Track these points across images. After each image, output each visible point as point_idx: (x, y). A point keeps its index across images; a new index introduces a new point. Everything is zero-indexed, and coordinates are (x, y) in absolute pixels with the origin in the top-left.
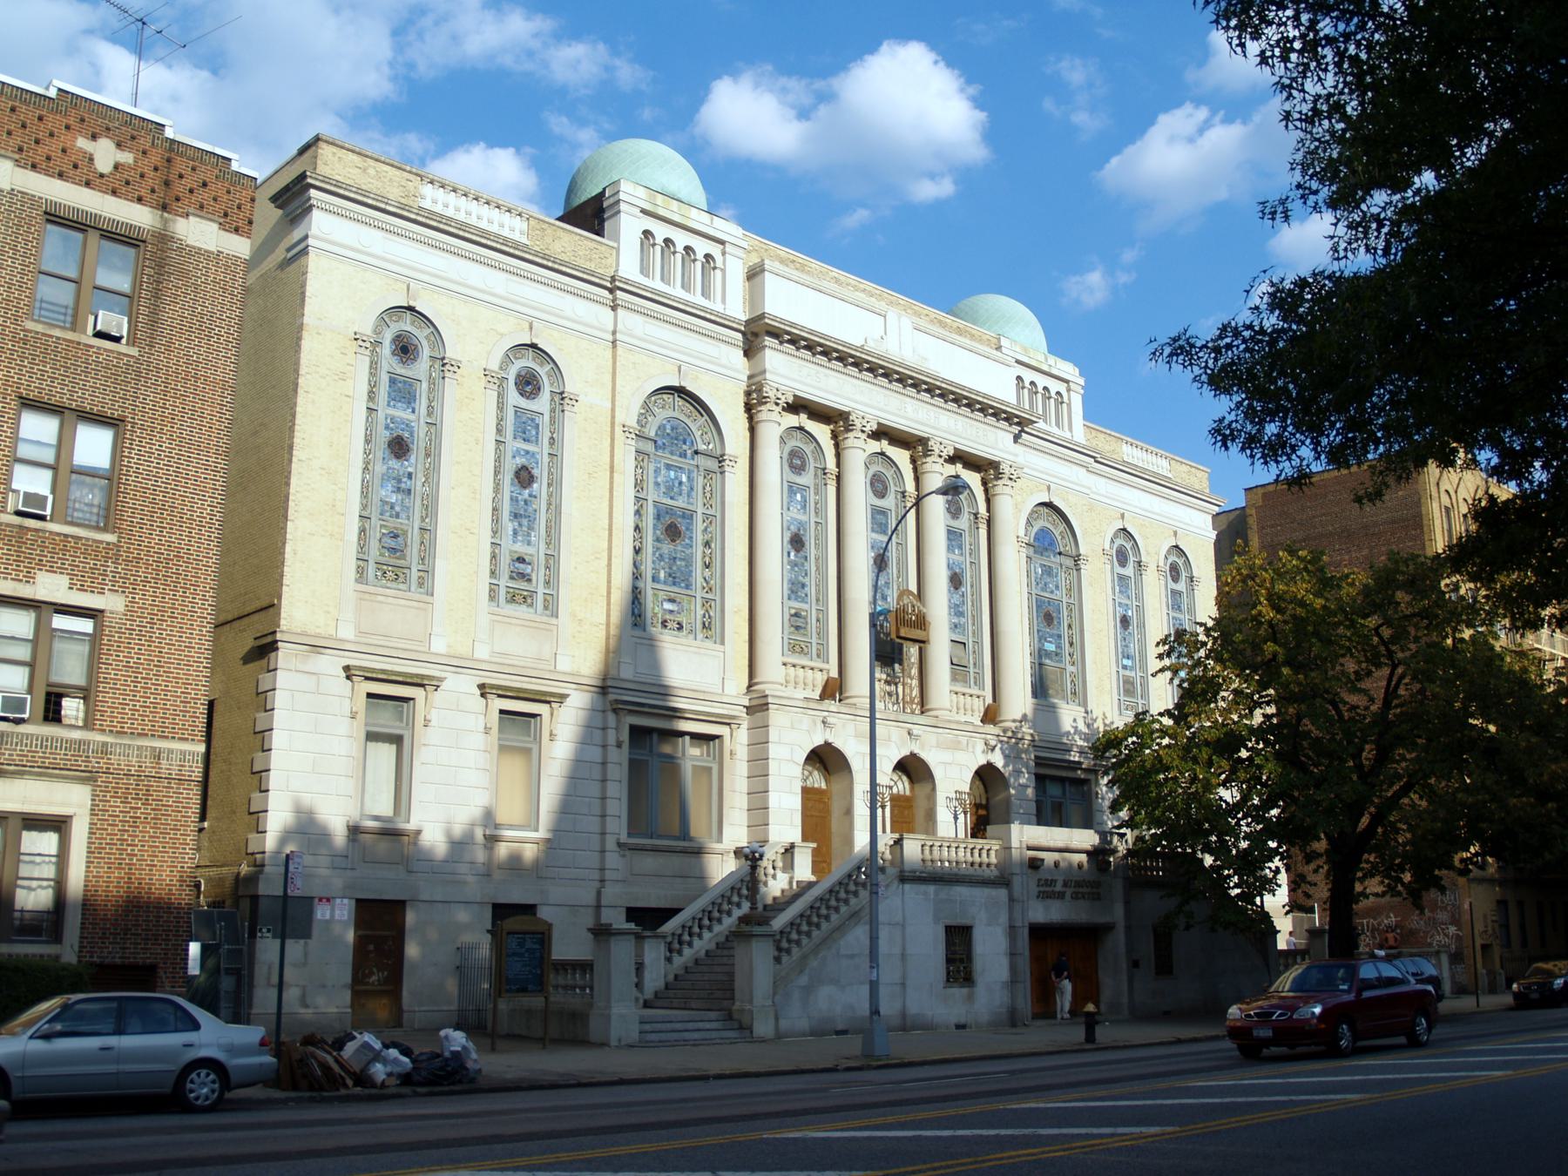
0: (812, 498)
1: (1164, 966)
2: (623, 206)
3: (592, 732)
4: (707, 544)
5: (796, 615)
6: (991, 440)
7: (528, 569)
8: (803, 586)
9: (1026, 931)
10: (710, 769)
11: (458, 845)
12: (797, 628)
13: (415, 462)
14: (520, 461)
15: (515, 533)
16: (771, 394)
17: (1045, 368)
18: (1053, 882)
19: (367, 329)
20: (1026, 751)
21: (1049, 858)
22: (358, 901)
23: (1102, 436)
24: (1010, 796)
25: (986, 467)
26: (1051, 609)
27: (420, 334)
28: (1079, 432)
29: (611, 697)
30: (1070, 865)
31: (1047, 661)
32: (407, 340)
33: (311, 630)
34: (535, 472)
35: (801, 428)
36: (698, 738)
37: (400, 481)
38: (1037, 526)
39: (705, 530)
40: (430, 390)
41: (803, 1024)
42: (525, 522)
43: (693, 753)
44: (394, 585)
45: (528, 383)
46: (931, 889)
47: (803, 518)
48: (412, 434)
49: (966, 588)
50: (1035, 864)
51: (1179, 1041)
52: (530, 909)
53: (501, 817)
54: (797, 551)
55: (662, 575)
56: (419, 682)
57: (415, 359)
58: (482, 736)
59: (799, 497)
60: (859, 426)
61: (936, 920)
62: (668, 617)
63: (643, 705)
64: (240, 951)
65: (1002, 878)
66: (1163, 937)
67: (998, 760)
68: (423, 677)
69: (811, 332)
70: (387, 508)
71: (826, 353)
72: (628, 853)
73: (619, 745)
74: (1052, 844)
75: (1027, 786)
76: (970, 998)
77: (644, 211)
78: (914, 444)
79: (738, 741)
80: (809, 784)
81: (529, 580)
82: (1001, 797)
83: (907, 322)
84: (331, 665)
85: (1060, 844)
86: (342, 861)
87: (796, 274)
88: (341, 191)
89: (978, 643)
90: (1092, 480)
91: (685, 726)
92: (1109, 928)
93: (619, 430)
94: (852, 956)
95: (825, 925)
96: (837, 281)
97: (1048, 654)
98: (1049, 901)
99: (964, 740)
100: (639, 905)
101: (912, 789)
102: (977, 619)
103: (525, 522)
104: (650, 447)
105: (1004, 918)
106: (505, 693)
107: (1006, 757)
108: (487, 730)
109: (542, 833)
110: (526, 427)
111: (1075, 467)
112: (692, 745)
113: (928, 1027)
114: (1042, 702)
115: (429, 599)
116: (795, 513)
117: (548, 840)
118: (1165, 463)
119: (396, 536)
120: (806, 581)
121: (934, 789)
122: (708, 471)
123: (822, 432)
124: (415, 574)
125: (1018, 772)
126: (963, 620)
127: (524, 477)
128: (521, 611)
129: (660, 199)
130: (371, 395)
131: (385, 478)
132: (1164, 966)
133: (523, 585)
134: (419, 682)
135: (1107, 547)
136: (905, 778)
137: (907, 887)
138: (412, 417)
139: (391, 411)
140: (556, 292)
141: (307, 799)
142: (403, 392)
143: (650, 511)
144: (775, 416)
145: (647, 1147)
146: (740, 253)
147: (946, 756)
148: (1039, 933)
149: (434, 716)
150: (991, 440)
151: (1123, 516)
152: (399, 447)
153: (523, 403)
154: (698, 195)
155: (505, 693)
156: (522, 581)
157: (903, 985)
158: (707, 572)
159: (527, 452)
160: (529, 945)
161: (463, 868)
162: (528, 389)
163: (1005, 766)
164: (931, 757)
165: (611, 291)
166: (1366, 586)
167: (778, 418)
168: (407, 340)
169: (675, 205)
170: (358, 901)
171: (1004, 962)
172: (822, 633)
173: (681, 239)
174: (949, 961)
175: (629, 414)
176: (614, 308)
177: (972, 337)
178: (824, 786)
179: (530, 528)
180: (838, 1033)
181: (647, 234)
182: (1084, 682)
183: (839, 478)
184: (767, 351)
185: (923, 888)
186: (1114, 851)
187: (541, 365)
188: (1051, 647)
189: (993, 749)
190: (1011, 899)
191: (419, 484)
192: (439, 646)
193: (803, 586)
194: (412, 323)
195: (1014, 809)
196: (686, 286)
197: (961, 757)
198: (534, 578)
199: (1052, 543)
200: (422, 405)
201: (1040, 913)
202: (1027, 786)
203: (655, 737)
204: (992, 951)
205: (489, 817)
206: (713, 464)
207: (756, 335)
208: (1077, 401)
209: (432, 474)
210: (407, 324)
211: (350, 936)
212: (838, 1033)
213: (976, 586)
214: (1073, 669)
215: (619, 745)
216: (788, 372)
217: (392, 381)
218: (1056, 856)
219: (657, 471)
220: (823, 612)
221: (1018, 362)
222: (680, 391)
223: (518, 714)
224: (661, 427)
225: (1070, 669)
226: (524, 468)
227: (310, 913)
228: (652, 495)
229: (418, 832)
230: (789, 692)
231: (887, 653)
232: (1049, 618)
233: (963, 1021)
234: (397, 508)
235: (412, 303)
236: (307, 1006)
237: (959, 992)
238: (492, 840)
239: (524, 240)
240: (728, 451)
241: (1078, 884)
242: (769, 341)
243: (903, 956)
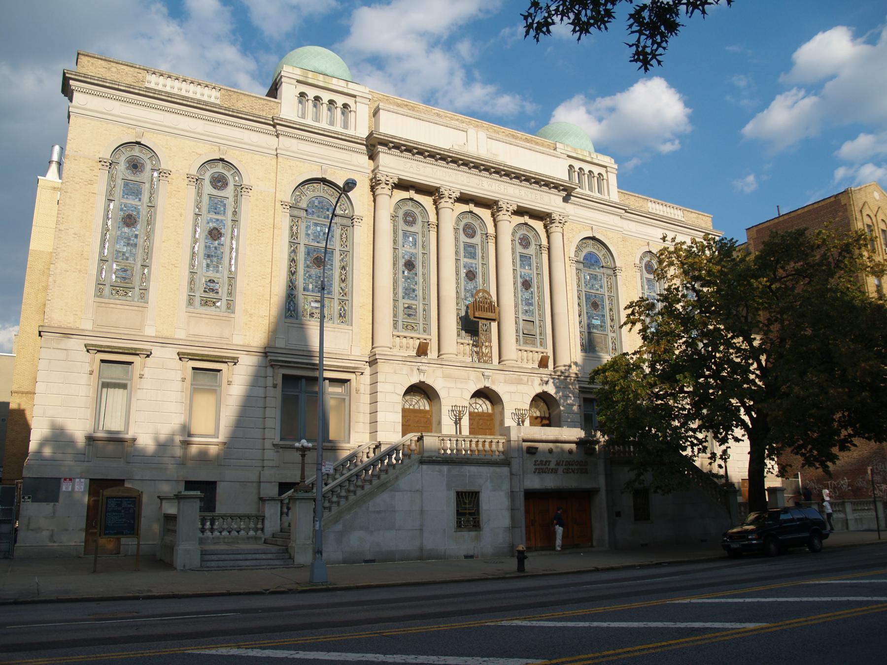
0: (420, 238)
1: (642, 513)
2: (283, 79)
3: (257, 379)
4: (611, 310)
5: (408, 307)
6: (550, 202)
7: (217, 286)
8: (414, 290)
9: (522, 494)
10: (344, 399)
11: (163, 446)
12: (409, 315)
13: (139, 229)
14: (211, 225)
15: (208, 266)
16: (383, 179)
17: (589, 159)
18: (548, 462)
19: (194, 171)
20: (572, 384)
21: (540, 446)
22: (91, 480)
23: (633, 198)
24: (561, 411)
25: (543, 217)
26: (597, 299)
27: (144, 156)
28: (613, 194)
29: (269, 358)
30: (563, 451)
31: (595, 331)
32: (134, 161)
33: (64, 324)
34: (223, 231)
35: (526, 224)
36: (333, 381)
37: (129, 239)
38: (585, 252)
39: (342, 259)
40: (482, 250)
41: (339, 556)
42: (215, 259)
43: (332, 390)
44: (124, 298)
45: (219, 181)
46: (445, 468)
47: (414, 251)
48: (138, 213)
49: (534, 289)
50: (532, 451)
51: (633, 567)
52: (120, 482)
53: (194, 431)
54: (410, 270)
55: (311, 286)
56: (134, 353)
57: (142, 171)
58: (86, 376)
59: (411, 239)
60: (505, 208)
61: (449, 488)
62: (314, 311)
63: (290, 362)
64: (11, 510)
65: (505, 460)
66: (641, 497)
67: (551, 389)
68: (136, 349)
69: (407, 140)
70: (120, 255)
71: (518, 177)
72: (281, 450)
73: (275, 386)
74: (544, 438)
75: (573, 405)
76: (478, 538)
77: (298, 81)
78: (490, 204)
79: (361, 383)
80: (407, 406)
81: (217, 293)
82: (556, 412)
83: (482, 135)
84: (171, 353)
85: (551, 438)
86: (81, 456)
87: (411, 113)
88: (89, 80)
89: (542, 320)
90: (626, 224)
91: (327, 374)
92: (596, 491)
93: (567, 259)
94: (379, 512)
95: (359, 492)
96: (438, 115)
97: (595, 327)
98: (544, 475)
99: (525, 378)
100: (288, 481)
101: (493, 409)
102: (541, 307)
103: (215, 259)
104: (581, 266)
105: (506, 486)
106: (193, 357)
107: (557, 387)
108: (183, 380)
109: (221, 438)
110: (216, 206)
111: (611, 216)
112: (330, 386)
113: (442, 557)
114: (591, 355)
115: (145, 305)
116: (408, 248)
117: (225, 443)
118: (680, 213)
119: (125, 271)
120: (416, 287)
121: (503, 408)
122: (344, 226)
123: (538, 225)
124: (421, 326)
125: (566, 397)
126: (531, 308)
127: (215, 234)
128: (211, 310)
129: (310, 75)
130: (457, 253)
131: (118, 239)
132: (642, 513)
133: (212, 295)
134: (134, 353)
135: (637, 262)
136: (487, 402)
137: (424, 467)
138: (139, 203)
139: (124, 201)
140: (237, 129)
141: (60, 421)
142: (216, 206)
143: (302, 250)
144: (507, 217)
145: (773, 586)
146: (367, 101)
147: (513, 388)
148: (531, 495)
149: (146, 372)
150: (550, 202)
151: (648, 244)
152: (129, 220)
153: (215, 192)
154: (347, 75)
155: (193, 357)
156: (211, 292)
157: (421, 530)
158: (343, 285)
159: (218, 220)
160: (124, 504)
161: (166, 460)
162: (219, 184)
163: (556, 393)
164: (499, 388)
165: (274, 126)
166: (832, 278)
167: (509, 219)
168: (134, 161)
169: (321, 77)
170: (91, 480)
171: (507, 515)
172: (427, 317)
173: (587, 168)
174: (459, 514)
175: (286, 194)
176: (277, 136)
177: (537, 144)
178: (427, 408)
179: (219, 263)
180: (366, 561)
181: (571, 166)
182: (621, 342)
183: (549, 249)
184: (381, 154)
185: (437, 467)
186: (598, 442)
187: (229, 171)
188: (596, 322)
189: (547, 383)
190: (511, 474)
191: (142, 240)
192: (150, 331)
193: (414, 290)
194: (223, 168)
195: (563, 419)
196: (591, 189)
197: (521, 388)
198: (220, 290)
199: (597, 261)
200: (145, 197)
201: (535, 482)
202: (573, 405)
203: (304, 381)
204: (497, 509)
205: (186, 431)
206: (610, 272)
207: (374, 145)
208: (613, 179)
209: (149, 236)
210: (220, 168)
211: (86, 499)
212: (366, 561)
213: (540, 288)
214: (613, 335)
215: (275, 386)
216: (393, 165)
217: (126, 185)
218: (551, 445)
219: (308, 227)
220: (426, 305)
221: (569, 156)
222: (593, 238)
223: (206, 368)
224: (311, 202)
225: (611, 335)
226: (215, 228)
227: (59, 487)
228: (303, 240)
229: (134, 440)
230: (395, 351)
231: (470, 326)
232: (595, 305)
233: (471, 553)
234: (127, 255)
235: (138, 140)
236: (54, 542)
237: (467, 535)
238: (186, 444)
239: (218, 102)
240: (617, 265)
241: (568, 463)
242: (380, 148)
243: (422, 512)
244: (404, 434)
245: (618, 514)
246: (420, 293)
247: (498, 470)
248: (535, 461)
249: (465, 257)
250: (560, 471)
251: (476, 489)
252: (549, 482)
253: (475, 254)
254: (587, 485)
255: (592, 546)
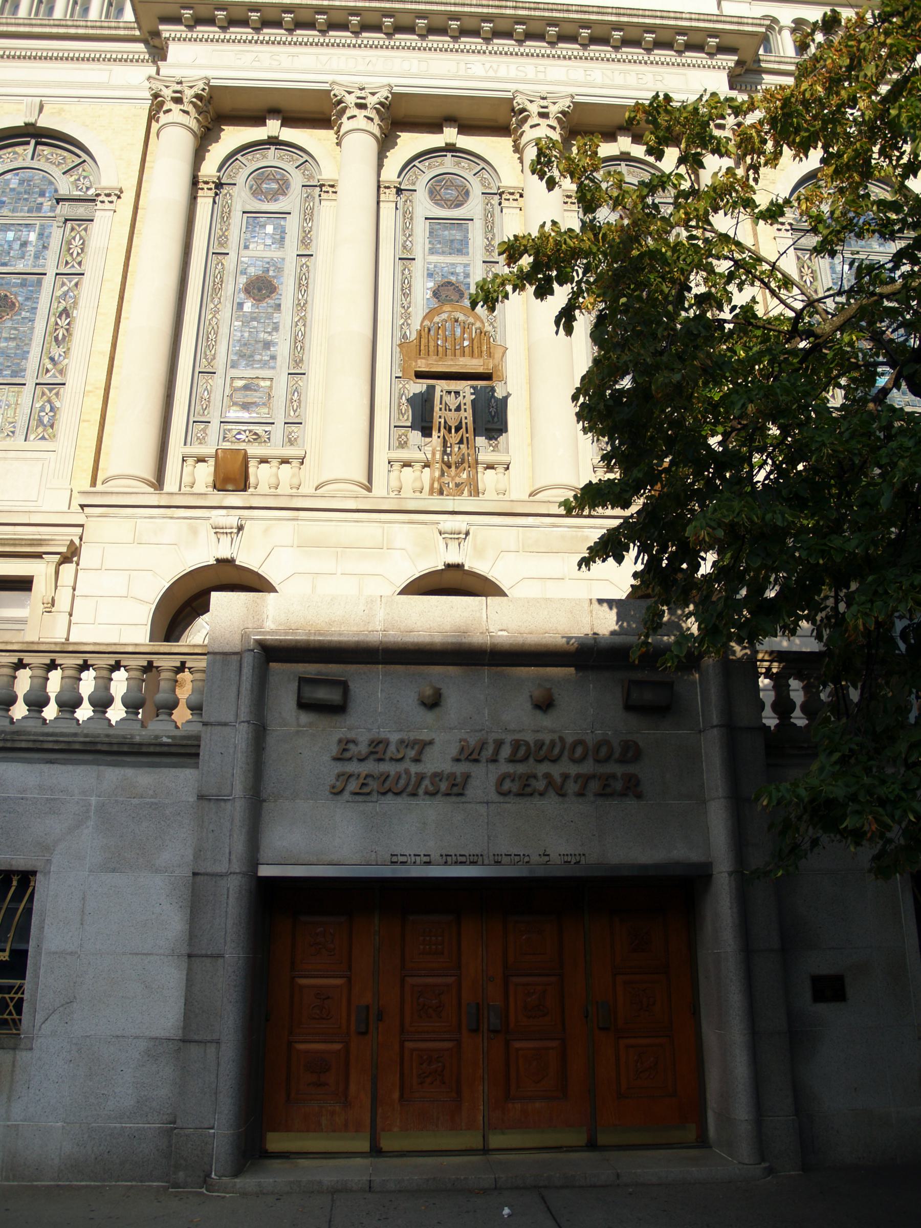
5: (246, 388)
8: (267, 345)
59: (270, 229)
158: (56, 351)
171: (171, 978)
244: (467, 777)
245: (830, 989)
246: (283, 349)
247: (144, 778)
248: (346, 744)
249: (432, 251)
250: (483, 779)
251: (20, 862)
252: (420, 840)
253: (465, 242)
254: (625, 843)
255: (702, 1141)
